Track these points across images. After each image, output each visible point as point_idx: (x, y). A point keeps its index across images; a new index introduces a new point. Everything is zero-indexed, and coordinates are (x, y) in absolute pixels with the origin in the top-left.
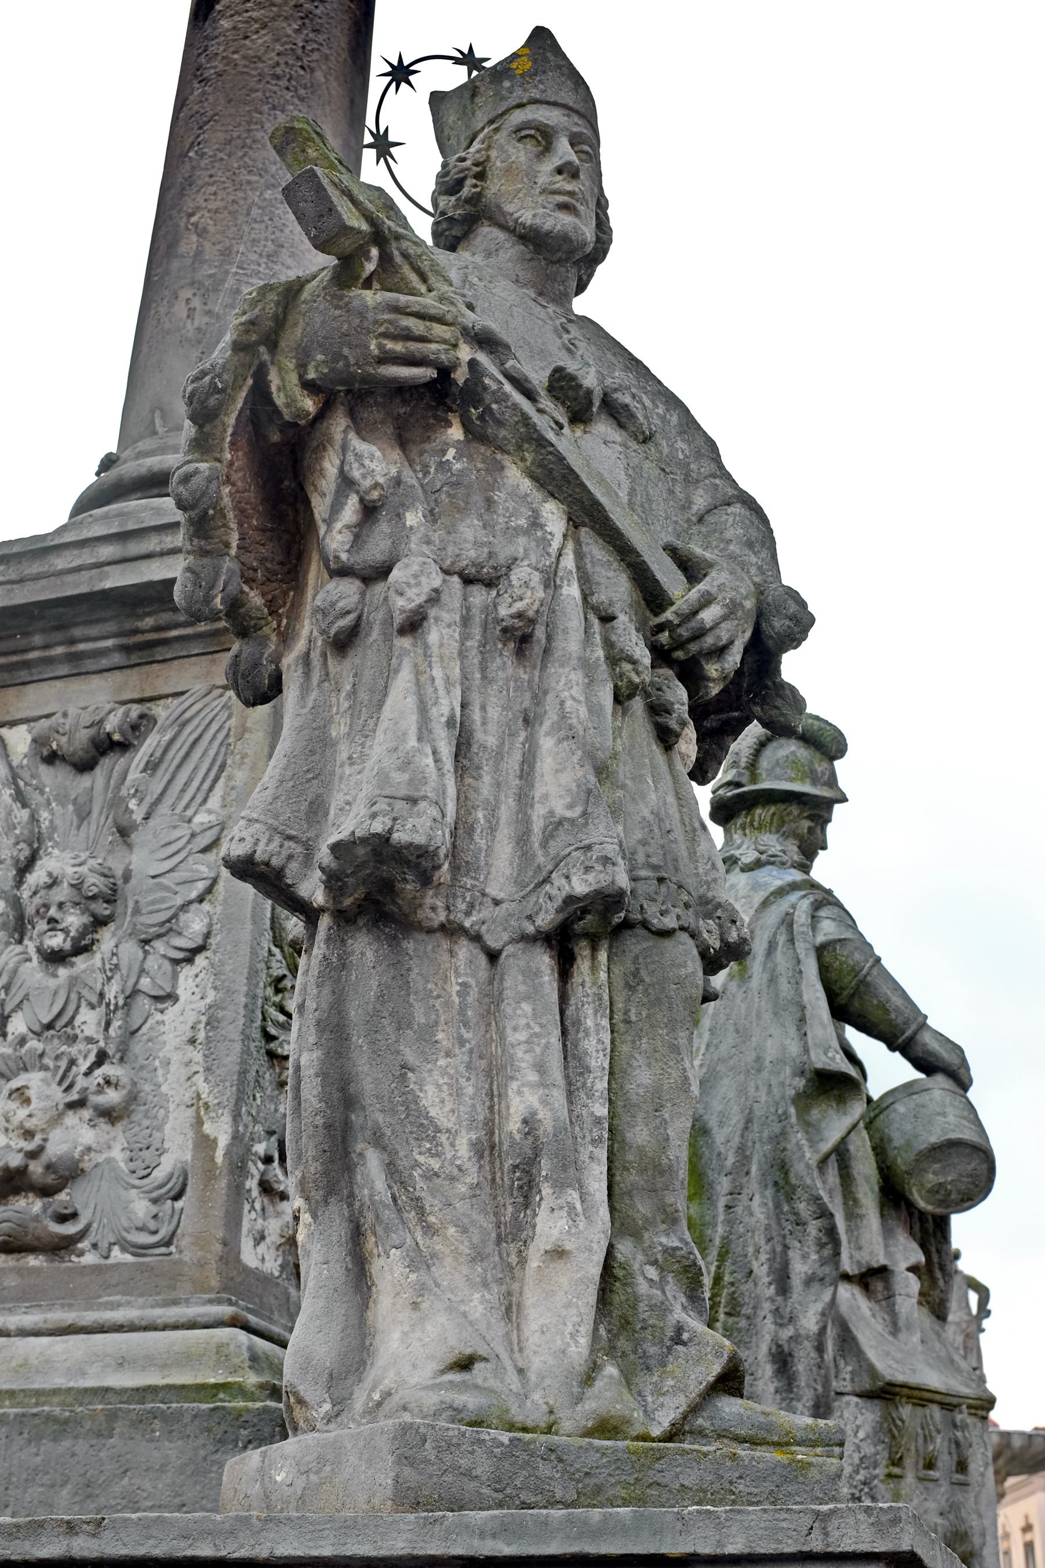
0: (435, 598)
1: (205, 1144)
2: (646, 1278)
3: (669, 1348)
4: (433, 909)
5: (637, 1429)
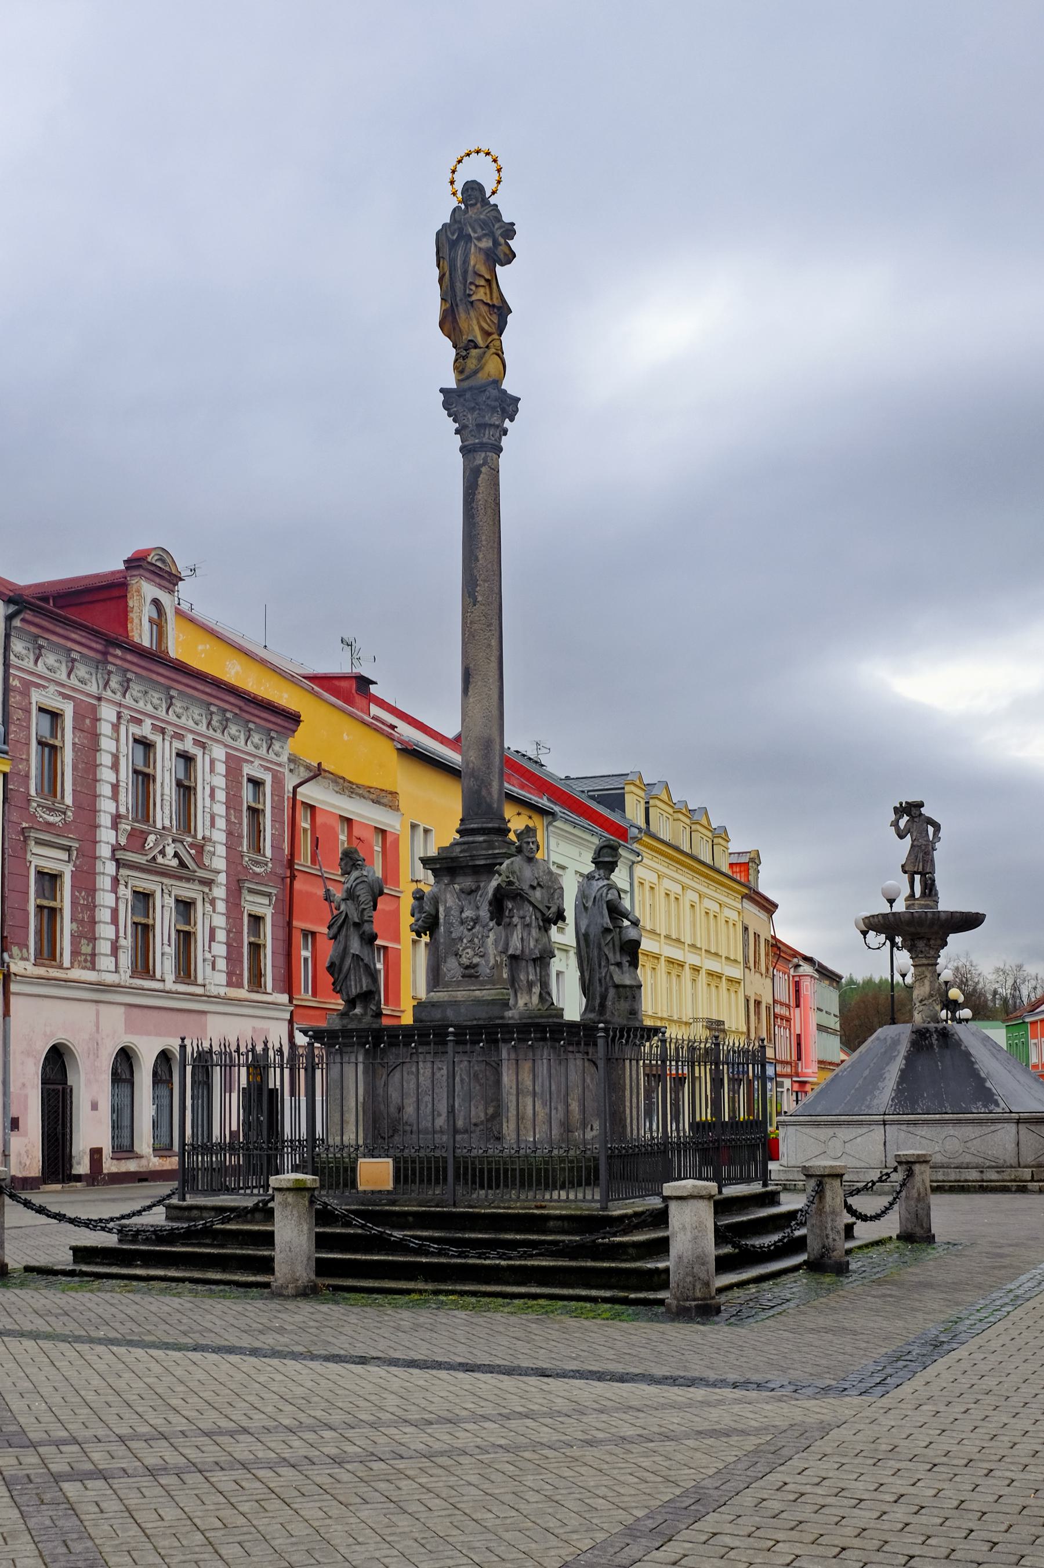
1: (496, 961)
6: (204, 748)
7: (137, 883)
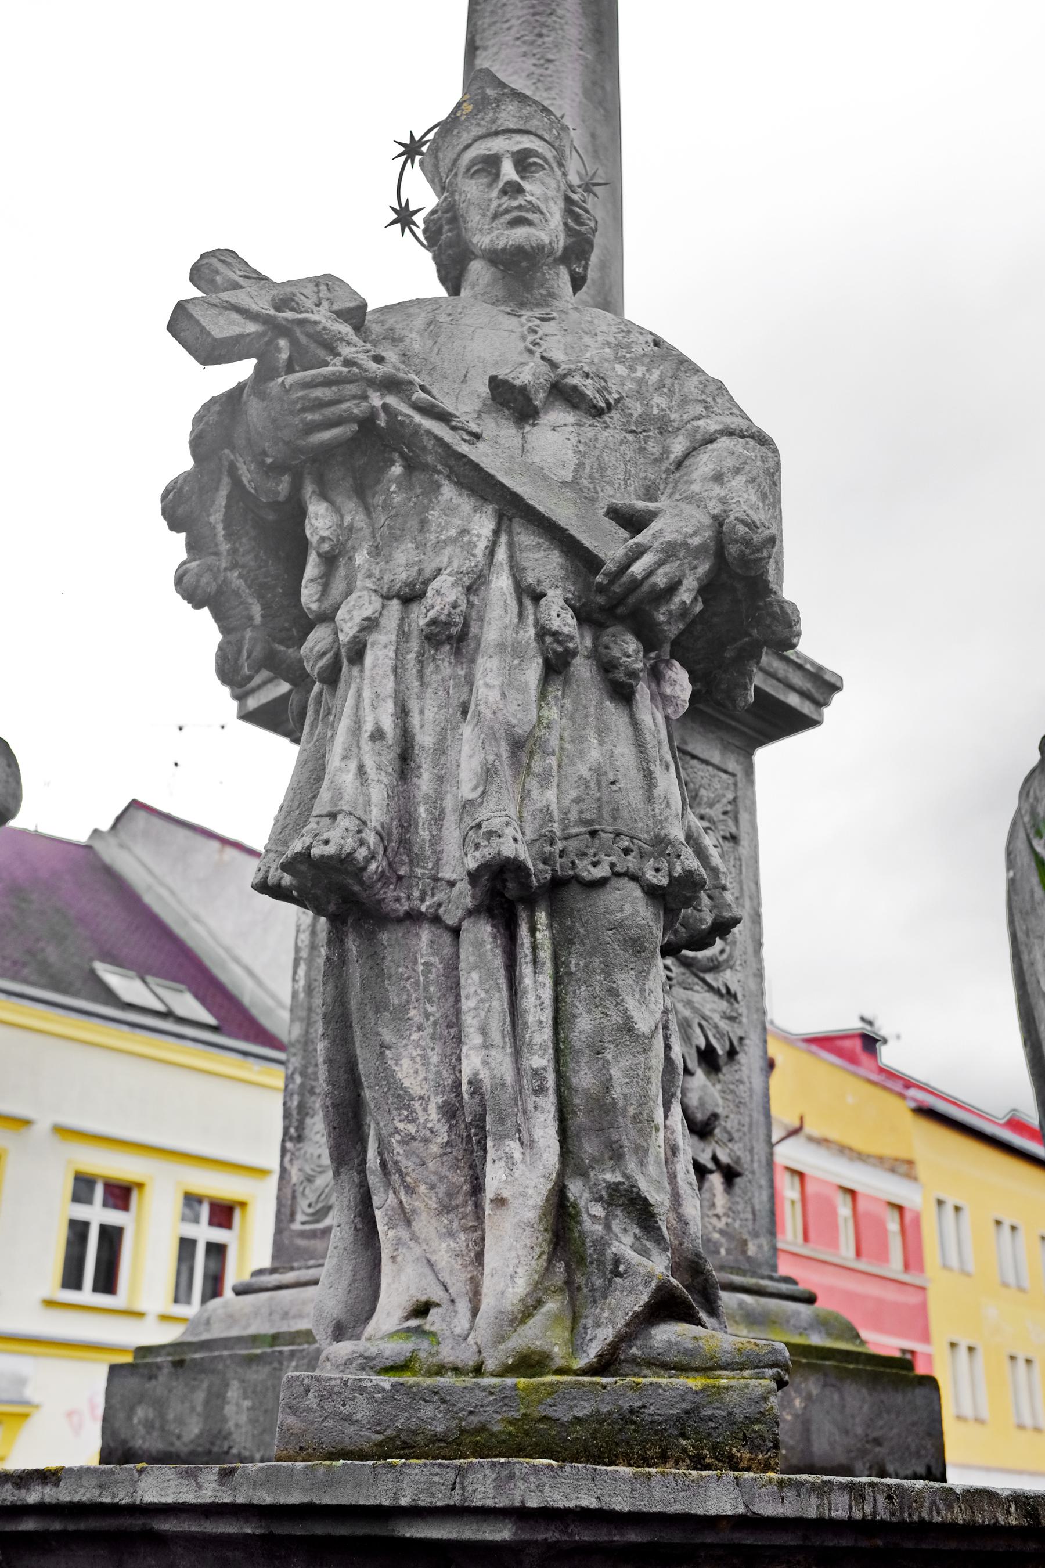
0: (371, 624)
2: (589, 1215)
3: (610, 1281)
4: (398, 900)
5: (559, 1362)
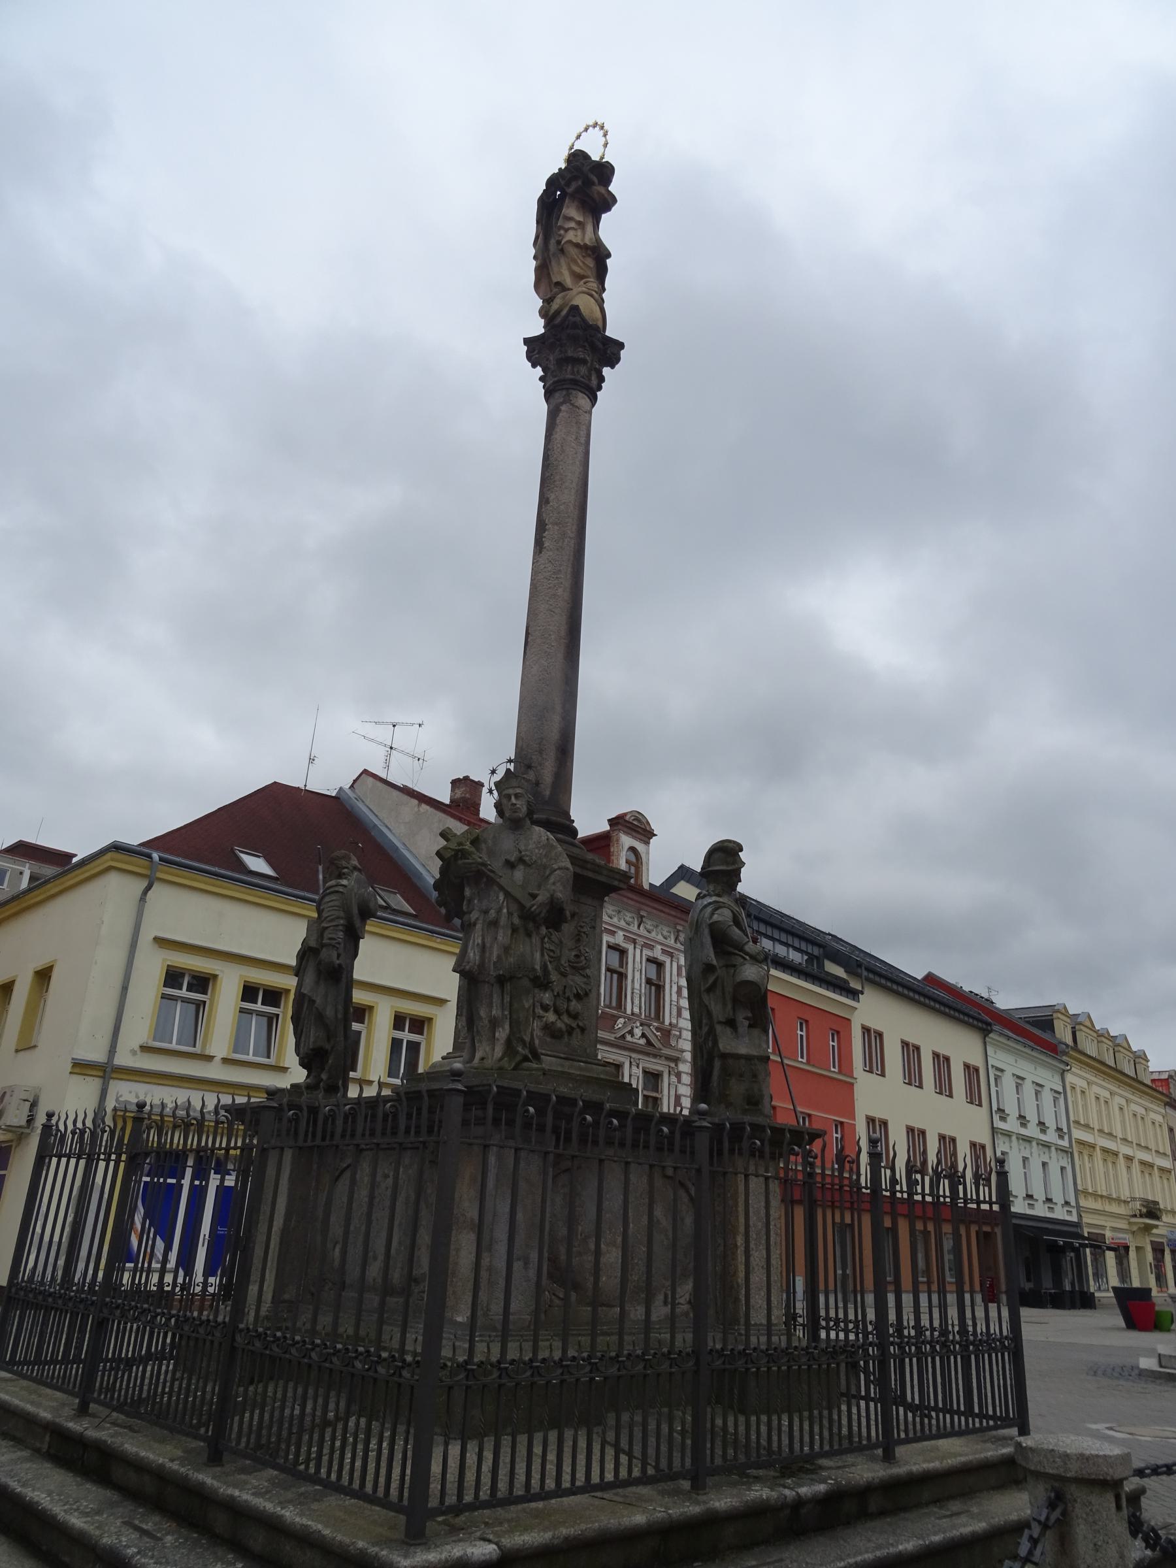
0: (477, 919)
6: (672, 957)
7: (647, 1065)
